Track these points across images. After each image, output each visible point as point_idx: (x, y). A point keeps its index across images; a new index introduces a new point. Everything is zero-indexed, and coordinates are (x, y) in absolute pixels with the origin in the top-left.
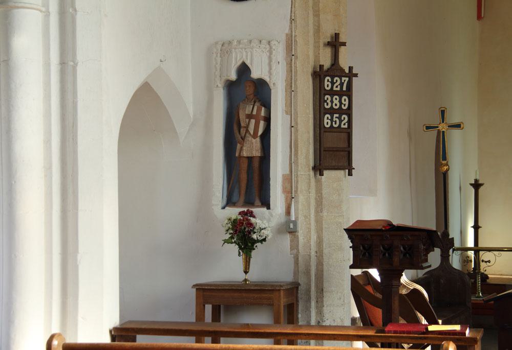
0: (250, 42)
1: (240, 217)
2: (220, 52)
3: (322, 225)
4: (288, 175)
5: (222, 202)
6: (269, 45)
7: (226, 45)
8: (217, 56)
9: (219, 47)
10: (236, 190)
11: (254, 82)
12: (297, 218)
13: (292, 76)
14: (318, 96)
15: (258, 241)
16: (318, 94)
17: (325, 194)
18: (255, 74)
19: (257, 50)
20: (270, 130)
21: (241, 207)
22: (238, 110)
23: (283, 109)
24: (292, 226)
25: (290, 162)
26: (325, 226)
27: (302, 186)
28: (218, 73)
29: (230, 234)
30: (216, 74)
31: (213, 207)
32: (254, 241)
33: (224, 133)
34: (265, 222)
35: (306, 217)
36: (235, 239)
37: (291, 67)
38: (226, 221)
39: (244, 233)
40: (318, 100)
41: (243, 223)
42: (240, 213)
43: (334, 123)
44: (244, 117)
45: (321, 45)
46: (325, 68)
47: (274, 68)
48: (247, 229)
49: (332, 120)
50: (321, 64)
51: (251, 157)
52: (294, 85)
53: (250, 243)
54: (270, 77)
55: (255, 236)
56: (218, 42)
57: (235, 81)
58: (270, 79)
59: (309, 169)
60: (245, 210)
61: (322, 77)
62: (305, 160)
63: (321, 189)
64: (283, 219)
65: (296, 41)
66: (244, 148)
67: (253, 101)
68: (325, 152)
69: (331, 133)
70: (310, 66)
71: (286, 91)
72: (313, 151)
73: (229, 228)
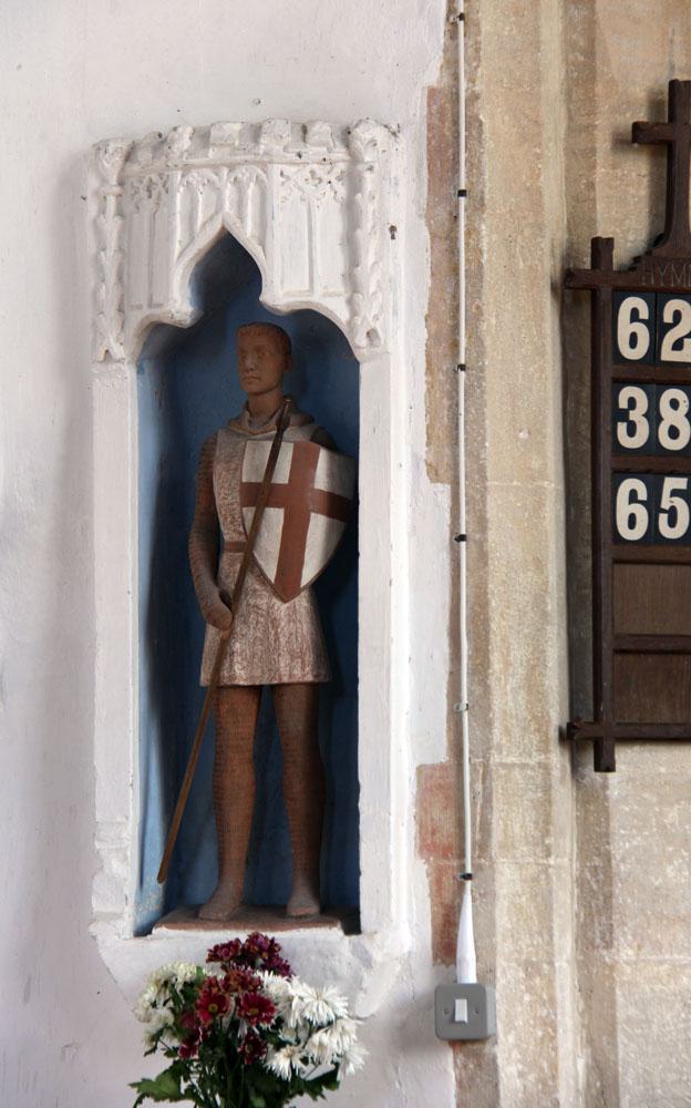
0: (256, 132)
1: (216, 972)
2: (117, 190)
3: (613, 1004)
4: (442, 767)
5: (138, 904)
6: (347, 145)
7: (144, 156)
8: (102, 211)
9: (112, 165)
10: (208, 852)
11: (280, 332)
12: (487, 972)
13: (456, 297)
14: (586, 392)
15: (297, 1085)
16: (587, 378)
17: (623, 860)
18: (281, 291)
19: (289, 170)
20: (356, 555)
21: (225, 927)
22: (209, 465)
23: (415, 456)
24: (462, 1011)
25: (450, 706)
26: (625, 1010)
27: (511, 820)
28: (109, 294)
29: (169, 1053)
30: (103, 294)
31: (93, 929)
32: (278, 1088)
33: (146, 580)
34: (331, 992)
35: (531, 968)
36: (194, 1079)
37: (453, 251)
38: (151, 993)
39: (229, 1047)
40: (586, 411)
41: (221, 1001)
42: (215, 954)
43: (663, 519)
44: (235, 497)
45: (603, 143)
46: (621, 254)
47: (368, 259)
48: (243, 1031)
49: (653, 505)
50: (599, 234)
51: (273, 688)
52: (469, 337)
53: (259, 1093)
54: (350, 302)
55: (281, 1063)
56: (106, 143)
57: (191, 328)
58: (354, 313)
59: (545, 741)
60: (243, 936)
61: (605, 294)
62: (522, 696)
63: (606, 836)
64: (422, 979)
65: (474, 123)
66: (237, 646)
67: (274, 419)
68: (619, 658)
69: (651, 569)
70: (546, 245)
71: (429, 370)
72: (564, 653)
73: (166, 1027)
